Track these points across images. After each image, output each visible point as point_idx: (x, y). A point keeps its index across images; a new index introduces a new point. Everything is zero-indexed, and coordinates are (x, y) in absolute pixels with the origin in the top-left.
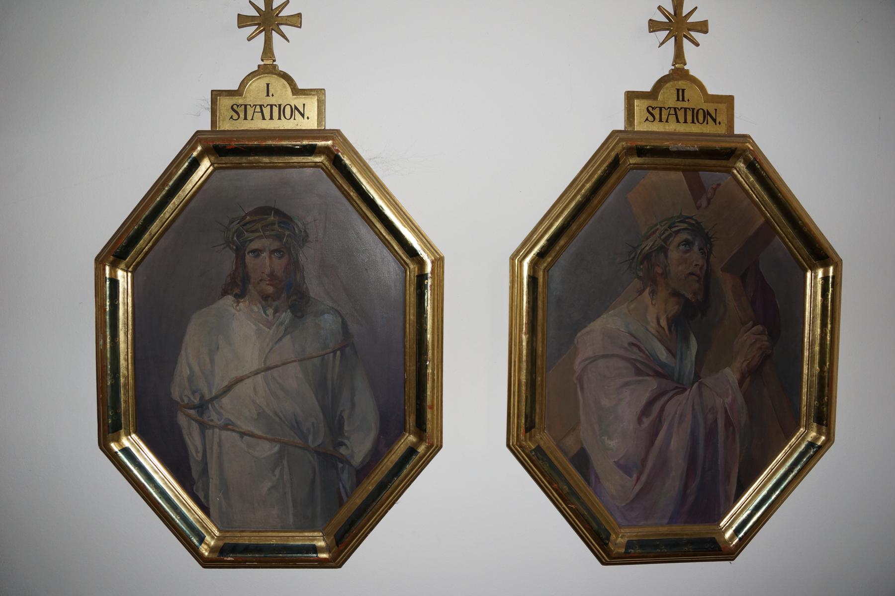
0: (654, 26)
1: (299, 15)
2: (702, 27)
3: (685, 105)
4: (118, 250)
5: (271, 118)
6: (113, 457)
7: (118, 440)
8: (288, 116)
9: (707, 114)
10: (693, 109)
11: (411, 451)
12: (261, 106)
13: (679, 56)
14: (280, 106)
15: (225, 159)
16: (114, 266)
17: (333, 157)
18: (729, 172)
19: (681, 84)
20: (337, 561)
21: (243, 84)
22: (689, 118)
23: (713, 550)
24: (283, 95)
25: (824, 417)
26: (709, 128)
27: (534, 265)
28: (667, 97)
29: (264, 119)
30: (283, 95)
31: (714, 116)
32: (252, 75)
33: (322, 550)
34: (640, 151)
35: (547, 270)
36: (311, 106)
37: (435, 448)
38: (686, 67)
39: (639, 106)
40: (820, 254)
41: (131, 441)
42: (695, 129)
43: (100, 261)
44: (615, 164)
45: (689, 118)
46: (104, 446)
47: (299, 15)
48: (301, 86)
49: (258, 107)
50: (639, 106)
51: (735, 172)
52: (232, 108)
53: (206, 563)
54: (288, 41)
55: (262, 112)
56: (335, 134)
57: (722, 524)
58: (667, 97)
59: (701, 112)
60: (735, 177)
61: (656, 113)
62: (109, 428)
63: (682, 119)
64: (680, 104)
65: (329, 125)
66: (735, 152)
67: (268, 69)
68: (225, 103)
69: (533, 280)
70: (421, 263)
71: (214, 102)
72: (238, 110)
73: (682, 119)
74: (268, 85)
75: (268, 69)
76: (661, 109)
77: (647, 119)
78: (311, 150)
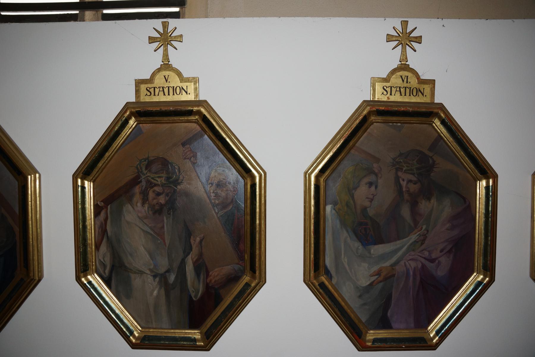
0: (152, 40)
1: (181, 36)
2: (418, 40)
3: (408, 85)
4: (86, 170)
5: (169, 95)
6: (442, 338)
7: (85, 276)
8: (415, 94)
9: (418, 91)
10: (173, 87)
11: (247, 285)
12: (163, 87)
13: (166, 56)
14: (410, 88)
15: (142, 119)
16: (83, 179)
17: (202, 117)
18: (431, 124)
19: (404, 73)
20: (207, 348)
21: (154, 75)
22: (408, 94)
23: (423, 344)
24: (175, 82)
25: (489, 269)
26: (184, 97)
27: (317, 177)
28: (396, 81)
29: (164, 95)
30: (175, 82)
31: (422, 91)
32: (159, 70)
33: (199, 341)
34: (379, 113)
35: (326, 181)
36: (191, 87)
37: (262, 281)
38: (407, 63)
39: (379, 87)
40: (485, 170)
41: (95, 280)
42: (414, 99)
43: (75, 177)
44: (365, 119)
45: (408, 94)
46: (78, 279)
47: (181, 36)
48: (185, 75)
49: (161, 88)
50: (143, 87)
51: (434, 125)
52: (147, 89)
53: (134, 346)
54: (177, 49)
55: (163, 91)
56: (204, 103)
57: (429, 328)
58: (396, 81)
59: (178, 88)
60: (434, 127)
61: (152, 90)
62: (82, 267)
63: (166, 93)
64: (166, 85)
65: (202, 98)
66: (432, 112)
67: (166, 66)
68: (143, 87)
69: (317, 187)
70: (253, 177)
71: (136, 86)
72: (150, 90)
73: (166, 93)
74: (165, 76)
75: (166, 66)
76: (154, 88)
77: (383, 93)
78: (190, 113)
